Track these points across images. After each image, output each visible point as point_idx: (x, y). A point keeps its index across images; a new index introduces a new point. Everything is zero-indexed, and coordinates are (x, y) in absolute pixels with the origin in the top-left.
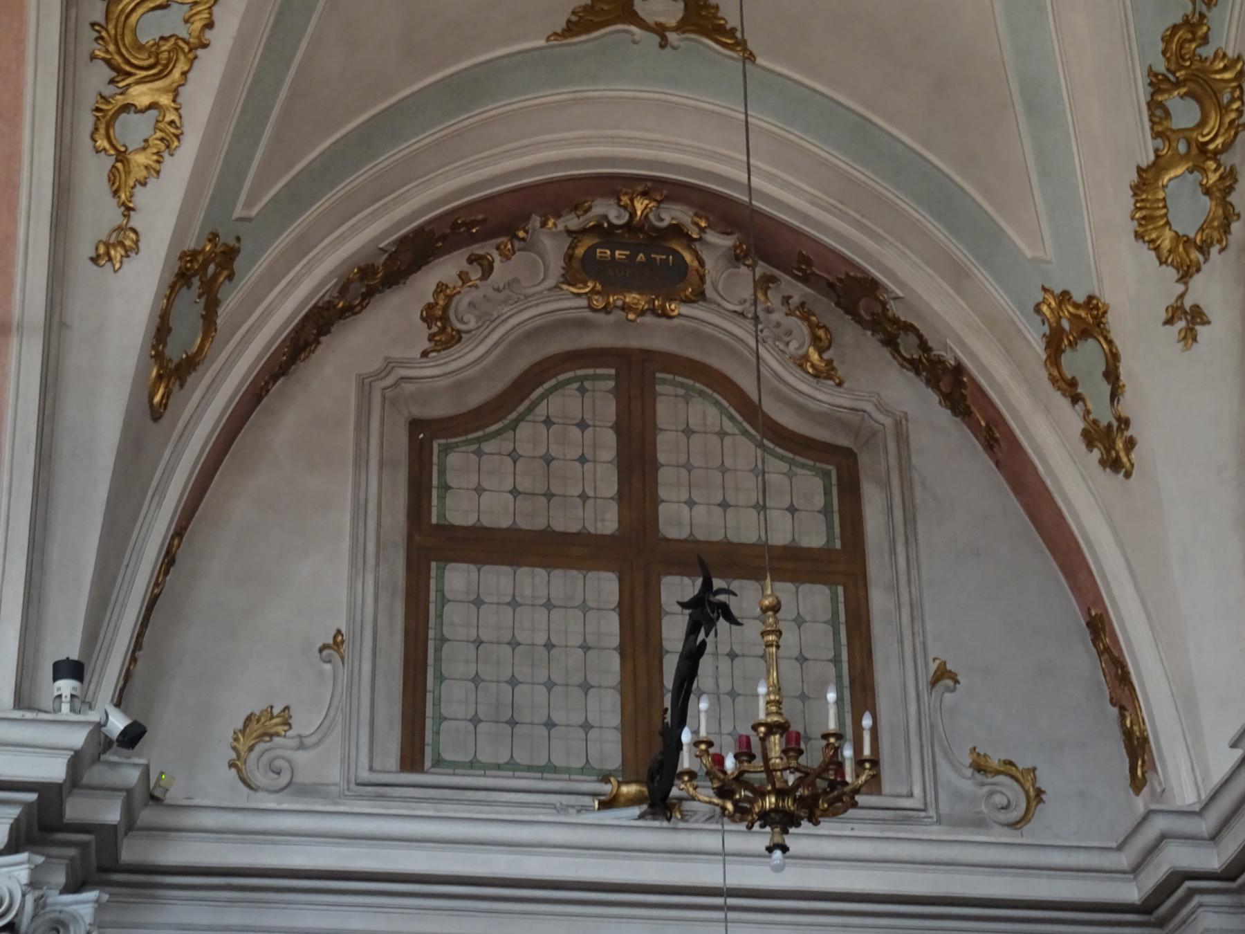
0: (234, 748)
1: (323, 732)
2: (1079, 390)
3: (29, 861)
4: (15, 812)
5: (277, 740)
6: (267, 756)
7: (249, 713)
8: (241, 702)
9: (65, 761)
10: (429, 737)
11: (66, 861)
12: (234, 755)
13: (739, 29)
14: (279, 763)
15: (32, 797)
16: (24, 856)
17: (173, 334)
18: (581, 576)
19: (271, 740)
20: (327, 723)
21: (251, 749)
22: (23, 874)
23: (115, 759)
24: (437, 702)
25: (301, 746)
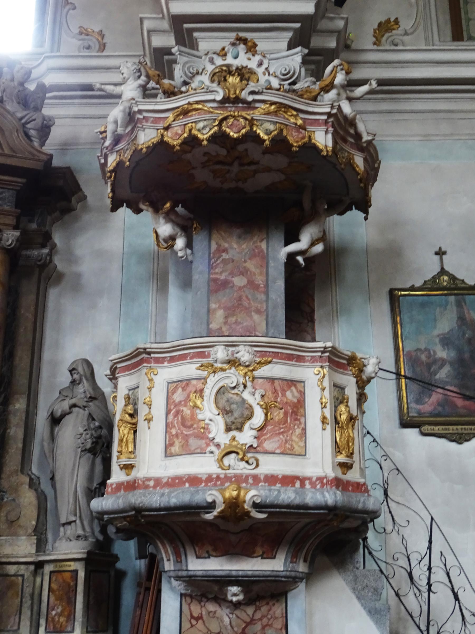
0: (374, 36)
1: (415, 28)
2: (122, 491)
3: (301, 51)
4: (289, 35)
5: (394, 32)
6: (390, 39)
7: (379, 21)
8: (374, 19)
9: (314, 4)
10: (464, 28)
11: (310, 72)
12: (375, 39)
13: (379, 48)
14: (396, 41)
15: (298, 25)
16: (299, 49)
17: (101, 499)
18: (104, 506)
19: (391, 32)
20: (416, 24)
21: (383, 36)
22: (299, 59)
23: (332, 15)
24: (466, 13)
25: (406, 34)
